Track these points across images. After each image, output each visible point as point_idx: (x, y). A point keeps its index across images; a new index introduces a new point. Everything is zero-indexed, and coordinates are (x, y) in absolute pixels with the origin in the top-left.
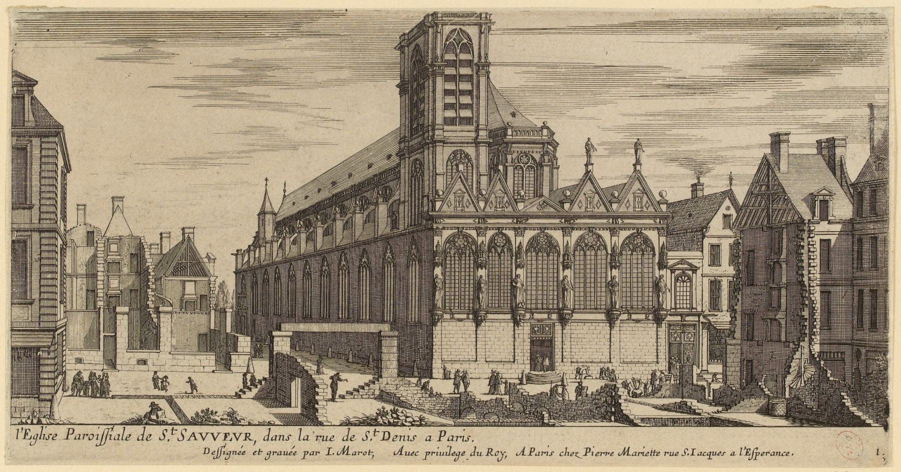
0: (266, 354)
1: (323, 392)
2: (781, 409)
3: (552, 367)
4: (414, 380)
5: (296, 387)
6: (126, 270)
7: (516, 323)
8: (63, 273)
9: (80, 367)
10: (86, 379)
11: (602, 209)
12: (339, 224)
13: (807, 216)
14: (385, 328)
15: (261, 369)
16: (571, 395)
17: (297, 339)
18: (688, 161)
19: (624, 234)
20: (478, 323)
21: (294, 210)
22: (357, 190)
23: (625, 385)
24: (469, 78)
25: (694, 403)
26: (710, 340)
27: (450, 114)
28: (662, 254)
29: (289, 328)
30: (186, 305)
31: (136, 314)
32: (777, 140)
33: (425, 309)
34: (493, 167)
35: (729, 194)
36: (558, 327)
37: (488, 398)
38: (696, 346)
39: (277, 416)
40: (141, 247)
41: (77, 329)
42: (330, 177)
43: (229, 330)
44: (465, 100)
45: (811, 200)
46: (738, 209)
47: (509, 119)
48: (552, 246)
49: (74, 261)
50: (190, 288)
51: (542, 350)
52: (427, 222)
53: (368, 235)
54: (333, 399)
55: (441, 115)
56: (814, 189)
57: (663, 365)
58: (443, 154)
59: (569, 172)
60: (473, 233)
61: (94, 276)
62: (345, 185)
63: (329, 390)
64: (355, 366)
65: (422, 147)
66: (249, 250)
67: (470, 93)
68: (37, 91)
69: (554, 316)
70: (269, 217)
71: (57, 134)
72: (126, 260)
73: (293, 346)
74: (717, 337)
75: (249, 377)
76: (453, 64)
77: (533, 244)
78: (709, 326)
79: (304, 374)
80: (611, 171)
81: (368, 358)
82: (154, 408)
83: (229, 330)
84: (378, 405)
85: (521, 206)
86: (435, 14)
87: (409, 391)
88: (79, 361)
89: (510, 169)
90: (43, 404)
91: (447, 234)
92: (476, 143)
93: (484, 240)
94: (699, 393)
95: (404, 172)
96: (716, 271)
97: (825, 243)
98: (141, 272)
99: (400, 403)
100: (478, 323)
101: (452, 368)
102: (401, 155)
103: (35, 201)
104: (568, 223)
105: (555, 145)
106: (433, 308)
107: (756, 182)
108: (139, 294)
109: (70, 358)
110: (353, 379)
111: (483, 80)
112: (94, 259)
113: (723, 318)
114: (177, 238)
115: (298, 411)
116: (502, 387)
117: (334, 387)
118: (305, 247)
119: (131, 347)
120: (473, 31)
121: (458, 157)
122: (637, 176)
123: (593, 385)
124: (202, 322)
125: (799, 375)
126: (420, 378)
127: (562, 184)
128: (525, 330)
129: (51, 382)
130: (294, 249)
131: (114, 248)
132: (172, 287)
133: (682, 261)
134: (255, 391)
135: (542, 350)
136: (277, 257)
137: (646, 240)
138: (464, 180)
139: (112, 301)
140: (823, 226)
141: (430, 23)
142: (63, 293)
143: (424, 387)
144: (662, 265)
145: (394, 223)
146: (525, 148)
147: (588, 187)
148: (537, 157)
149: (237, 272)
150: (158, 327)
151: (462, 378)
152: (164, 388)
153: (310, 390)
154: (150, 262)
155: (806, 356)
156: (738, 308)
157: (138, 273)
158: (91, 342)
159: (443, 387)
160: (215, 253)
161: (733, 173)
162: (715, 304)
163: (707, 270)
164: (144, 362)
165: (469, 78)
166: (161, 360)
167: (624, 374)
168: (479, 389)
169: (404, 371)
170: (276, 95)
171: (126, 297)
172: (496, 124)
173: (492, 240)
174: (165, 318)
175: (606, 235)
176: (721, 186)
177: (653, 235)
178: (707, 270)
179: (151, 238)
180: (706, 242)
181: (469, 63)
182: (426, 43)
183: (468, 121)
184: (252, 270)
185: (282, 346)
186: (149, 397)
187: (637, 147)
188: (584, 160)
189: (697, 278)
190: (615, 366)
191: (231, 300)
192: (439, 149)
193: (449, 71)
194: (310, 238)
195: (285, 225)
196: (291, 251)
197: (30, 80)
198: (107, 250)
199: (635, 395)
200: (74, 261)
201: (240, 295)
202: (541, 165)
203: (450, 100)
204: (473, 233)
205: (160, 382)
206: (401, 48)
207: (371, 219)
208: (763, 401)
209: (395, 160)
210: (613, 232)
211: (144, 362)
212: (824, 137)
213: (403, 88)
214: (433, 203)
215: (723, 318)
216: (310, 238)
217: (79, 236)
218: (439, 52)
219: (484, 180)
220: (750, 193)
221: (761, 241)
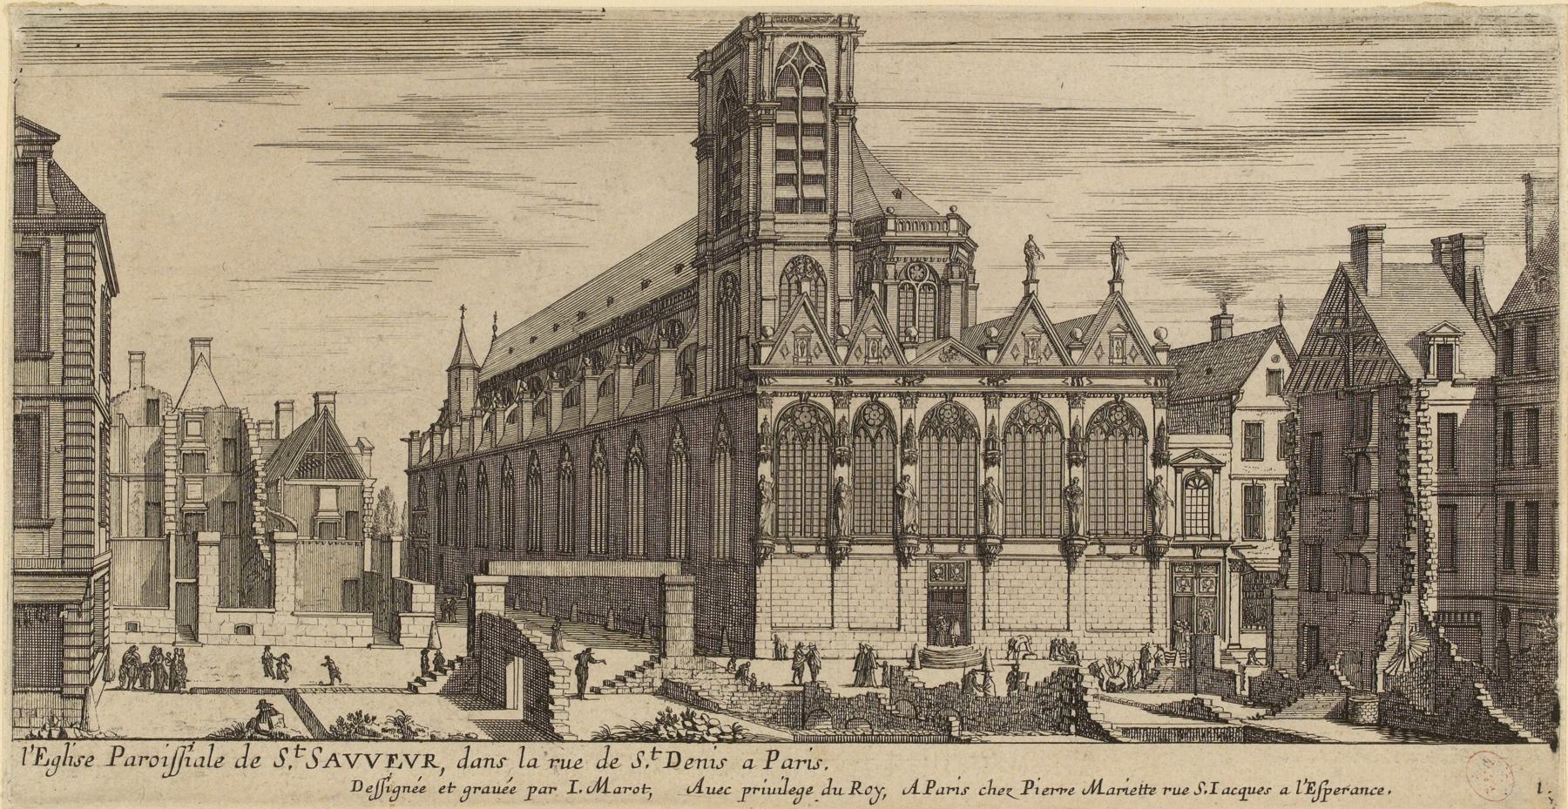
0: (462, 616)
1: (563, 683)
2: (1369, 713)
3: (965, 639)
4: (723, 661)
5: (515, 674)
6: (215, 467)
7: (903, 560)
8: (105, 473)
9: (134, 638)
10: (145, 659)
11: (1054, 360)
12: (591, 387)
13: (1415, 373)
14: (672, 569)
15: (454, 641)
16: (1000, 688)
17: (516, 590)
18: (1205, 276)
19: (1092, 405)
20: (835, 560)
22: (623, 326)
23: (1095, 670)
24: (820, 130)
25: (1216, 702)
27: (787, 192)
28: (1159, 439)
29: (502, 570)
30: (320, 529)
31: (233, 545)
32: (1362, 239)
33: (742, 536)
34: (862, 287)
35: (1277, 334)
36: (977, 568)
39: (481, 724)
40: (241, 427)
41: (129, 572)
42: (575, 304)
43: (396, 573)
44: (813, 168)
45: (1422, 344)
48: (965, 425)
49: (124, 451)
50: (328, 499)
51: (949, 609)
52: (744, 383)
53: (641, 405)
54: (580, 695)
56: (1426, 325)
57: (1162, 636)
58: (774, 263)
59: (995, 296)
60: (827, 403)
61: (160, 478)
62: (600, 318)
63: (574, 679)
65: (737, 250)
67: (821, 155)
68: (59, 153)
69: (970, 549)
70: (466, 375)
71: (94, 229)
72: (216, 450)
73: (509, 602)
74: (1257, 585)
75: (431, 655)
76: (791, 104)
77: (933, 422)
78: (1243, 566)
79: (529, 650)
80: (1070, 294)
81: (641, 622)
82: (265, 710)
83: (396, 573)
84: (659, 705)
86: (759, 17)
87: (714, 680)
88: (133, 627)
89: (892, 291)
91: (780, 403)
92: (833, 244)
94: (1225, 683)
95: (706, 295)
97: (1447, 419)
98: (242, 471)
100: (835, 560)
101: (790, 640)
102: (699, 264)
103: (56, 346)
104: (995, 384)
105: (972, 248)
107: (1325, 313)
110: (616, 660)
111: (844, 133)
112: (160, 443)
113: (1267, 553)
114: (304, 412)
115: (519, 715)
118: (530, 427)
119: (223, 603)
120: (826, 47)
121: (801, 268)
122: (1116, 302)
123: (1038, 670)
124: (350, 559)
125: (1401, 653)
126: (733, 658)
127: (983, 317)
128: (918, 573)
129: (83, 665)
130: (512, 430)
131: (194, 428)
132: (296, 498)
133: (1195, 452)
134: (442, 680)
135: (949, 609)
136: (481, 444)
137: (1132, 415)
138: (811, 309)
139: (192, 522)
140: (1444, 390)
141: (750, 33)
142: (104, 509)
143: (740, 674)
144: (1159, 459)
145: (688, 386)
146: (919, 252)
147: (1030, 320)
148: (940, 268)
149: (410, 472)
150: (271, 569)
151: (807, 658)
152: (282, 676)
154: (258, 454)
155: (1413, 618)
156: (1294, 534)
158: (154, 594)
159: (774, 674)
160: (371, 437)
163: (1239, 467)
164: (248, 630)
165: (820, 130)
166: (276, 625)
167: (1092, 650)
168: (837, 677)
169: (705, 645)
170: (481, 159)
171: (216, 516)
172: (866, 212)
173: (861, 414)
175: (1061, 405)
177: (1143, 406)
178: (1239, 467)
179: (260, 411)
180: (1238, 418)
181: (820, 103)
182: (744, 68)
183: (819, 205)
184: (438, 467)
185: (490, 601)
186: (255, 691)
187: (1116, 250)
189: (1221, 482)
190: (1077, 636)
191: (401, 521)
192: (767, 255)
193: (785, 117)
194: (540, 412)
195: (495, 389)
196: (507, 434)
197: (47, 133)
198: (182, 432)
199: (1112, 688)
200: (124, 451)
201: (416, 512)
203: (787, 168)
204: (827, 403)
205: (275, 665)
206: (699, 76)
207: (646, 378)
208: (1337, 699)
210: (1074, 400)
211: (248, 630)
212: (1445, 233)
213: (703, 147)
214: (757, 349)
215: (1267, 553)
216: (540, 412)
217: (132, 407)
218: (766, 84)
219: (846, 309)
220: (1315, 332)
221: (1334, 416)
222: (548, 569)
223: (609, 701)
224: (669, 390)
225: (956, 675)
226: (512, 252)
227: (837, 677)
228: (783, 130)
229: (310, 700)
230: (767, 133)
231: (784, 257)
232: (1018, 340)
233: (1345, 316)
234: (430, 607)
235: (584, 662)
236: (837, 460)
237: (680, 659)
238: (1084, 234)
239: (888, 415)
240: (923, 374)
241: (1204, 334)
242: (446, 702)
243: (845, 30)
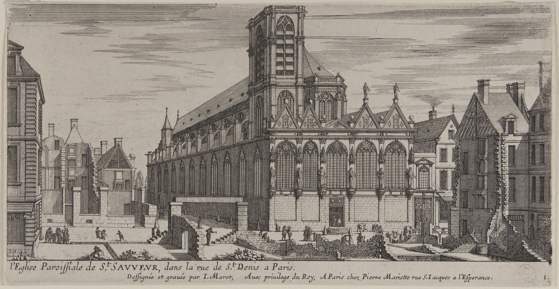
0: (166, 217)
1: (202, 240)
2: (484, 251)
3: (343, 224)
5: (185, 237)
6: (79, 164)
7: (321, 197)
9: (50, 224)
10: (54, 232)
11: (374, 127)
12: (212, 136)
13: (500, 131)
14: (240, 200)
15: (163, 225)
16: (355, 241)
17: (185, 207)
18: (427, 97)
19: (387, 142)
20: (297, 197)
21: (184, 127)
22: (223, 115)
23: (388, 235)
24: (292, 46)
25: (430, 247)
27: (280, 68)
28: (411, 155)
29: (180, 200)
30: (116, 186)
31: (86, 192)
32: (482, 84)
33: (265, 188)
34: (306, 102)
35: (452, 118)
36: (346, 200)
39: (173, 254)
40: (88, 150)
41: (49, 201)
42: (206, 107)
43: (143, 201)
44: (289, 59)
45: (503, 121)
48: (343, 149)
49: (47, 159)
50: (119, 175)
51: (337, 214)
52: (266, 135)
53: (229, 143)
56: (505, 114)
57: (411, 223)
58: (276, 93)
59: (353, 104)
60: (294, 142)
62: (215, 112)
63: (206, 238)
64: (221, 223)
65: (263, 88)
67: (292, 55)
68: (24, 53)
69: (344, 193)
70: (168, 132)
71: (36, 80)
72: (80, 158)
73: (183, 212)
74: (445, 206)
75: (156, 230)
77: (331, 149)
78: (440, 199)
79: (190, 228)
80: (379, 104)
81: (231, 220)
82: (97, 250)
83: (143, 201)
84: (236, 247)
85: (323, 125)
86: (270, 7)
87: (255, 239)
88: (50, 221)
89: (317, 102)
90: (27, 248)
91: (278, 142)
92: (296, 86)
93: (301, 146)
94: (434, 240)
95: (252, 104)
97: (512, 148)
98: (89, 165)
100: (297, 197)
101: (281, 225)
102: (249, 93)
103: (22, 122)
104: (353, 135)
105: (345, 87)
107: (469, 110)
108: (87, 180)
110: (220, 232)
111: (300, 47)
112: (60, 156)
113: (448, 194)
114: (111, 145)
118: (190, 150)
119: (82, 212)
120: (294, 17)
121: (285, 95)
122: (395, 106)
123: (368, 236)
124: (126, 196)
125: (496, 230)
126: (261, 231)
127: (349, 112)
128: (326, 202)
129: (32, 234)
130: (184, 151)
132: (108, 175)
133: (423, 159)
134: (159, 239)
135: (337, 214)
136: (173, 156)
137: (401, 146)
139: (71, 184)
140: (511, 137)
141: (267, 12)
142: (40, 179)
143: (264, 237)
144: (410, 162)
145: (246, 135)
146: (326, 89)
147: (365, 113)
148: (334, 95)
150: (99, 200)
151: (287, 231)
152: (103, 238)
153: (194, 238)
155: (500, 217)
156: (458, 188)
157: (87, 166)
158: (57, 209)
159: (276, 236)
160: (134, 153)
161: (455, 104)
163: (439, 164)
164: (91, 222)
165: (292, 46)
166: (100, 220)
167: (387, 229)
168: (298, 238)
169: (251, 227)
170: (173, 56)
171: (79, 181)
172: (308, 75)
173: (306, 146)
174: (103, 194)
175: (376, 143)
176: (448, 113)
177: (405, 143)
178: (439, 164)
179: (95, 144)
180: (438, 147)
181: (292, 37)
182: (265, 24)
183: (291, 72)
184: (158, 164)
186: (93, 243)
187: (395, 88)
189: (432, 169)
190: (382, 223)
191: (145, 183)
193: (280, 42)
194: (194, 145)
195: (178, 137)
196: (182, 153)
197: (19, 46)
198: (68, 152)
199: (394, 242)
200: (47, 159)
201: (150, 180)
203: (280, 59)
205: (101, 234)
206: (250, 27)
207: (231, 133)
208: (473, 246)
210: (381, 141)
211: (91, 222)
212: (511, 82)
213: (251, 52)
214: (270, 123)
215: (448, 194)
216: (194, 145)
217: (50, 143)
218: (273, 30)
219: (301, 109)
220: (465, 117)
221: (472, 146)
222: (197, 200)
224: (239, 137)
228: (279, 46)
230: (273, 47)
235: (209, 233)
236: (298, 162)
237: (243, 231)
239: (316, 146)
242: (161, 247)
243: (301, 11)
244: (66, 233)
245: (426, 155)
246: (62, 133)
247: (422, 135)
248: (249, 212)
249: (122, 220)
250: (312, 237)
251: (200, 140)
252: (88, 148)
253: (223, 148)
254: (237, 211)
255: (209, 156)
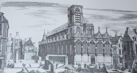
0: (44, 60)
1: (55, 67)
2: (132, 71)
3: (95, 63)
4: (71, 65)
5: (50, 66)
6: (18, 45)
7: (89, 56)
8: (7, 46)
9: (9, 63)
10: (10, 65)
11: (102, 38)
12: (58, 38)
13: (133, 40)
14: (66, 56)
15: (43, 63)
16: (98, 68)
17: (50, 57)
18: (114, 31)
19: (105, 42)
20: (82, 55)
21: (50, 35)
22: (61, 32)
23: (107, 67)
24: (79, 16)
25: (118, 70)
26: (120, 59)
27: (77, 21)
28: (111, 45)
29: (48, 55)
30: (29, 51)
31: (20, 53)
32: (127, 28)
33: (73, 53)
34: (84, 30)
35: (121, 36)
36: (95, 57)
37: (84, 68)
38: (117, 60)
39: (46, 71)
40: (21, 41)
41: (9, 55)
42: (56, 30)
43: (37, 56)
44: (79, 19)
45: (133, 38)
46: (122, 39)
47: (86, 22)
48: (94, 43)
49: (9, 43)
50: (30, 48)
51: (93, 60)
52: (73, 38)
53: (63, 39)
54: (56, 68)
55: (75, 21)
56: (134, 36)
57: (113, 63)
58: (75, 27)
59: (96, 32)
60: (81, 40)
61: (12, 46)
62: (58, 31)
63: (56, 67)
64: (61, 63)
65: (72, 26)
66: (41, 42)
67: (80, 18)
68: (4, 15)
69: (95, 55)
70: (45, 36)
71: (7, 22)
72: (19, 43)
73: (49, 59)
74: (121, 59)
75: (41, 64)
76: (76, 13)
77: (91, 43)
78: (119, 57)
79: (51, 64)
80: (103, 32)
81: (63, 61)
82: (23, 70)
83: (37, 56)
84: (65, 69)
85: (88, 36)
86: (74, 5)
87: (70, 67)
88: (9, 61)
89: (86, 30)
90: (2, 70)
91: (76, 40)
92: (81, 26)
93: (82, 41)
94: (119, 68)
95: (69, 30)
96: (120, 48)
97: (136, 45)
98: (21, 46)
99: (69, 69)
100: (82, 55)
101: (78, 63)
102: (68, 27)
103: (2, 33)
104: (96, 39)
105: (94, 27)
106: (74, 53)
107: (125, 35)
108: (21, 49)
109: (7, 61)
110: (60, 65)
111: (82, 16)
112: (12, 43)
113: (121, 56)
114: (28, 39)
115: (50, 70)
116: (86, 66)
117: (57, 66)
118: (51, 41)
119: (19, 59)
120: (80, 8)
121: (78, 28)
122: (107, 32)
123: (102, 66)
124: (32, 54)
125: (134, 66)
126: (72, 65)
127: (95, 33)
128: (90, 57)
129: (3, 66)
130: (50, 42)
131: (16, 41)
132: (27, 48)
133: (115, 46)
134: (42, 67)
135: (93, 60)
136: (46, 43)
137: (109, 43)
138: (79, 32)
139: (16, 50)
140: (135, 42)
141: (73, 6)
142: (7, 49)
143: (73, 66)
144: (111, 47)
145: (67, 38)
146: (89, 27)
147: (99, 34)
148: (91, 29)
149: (39, 46)
150: (24, 55)
151: (79, 65)
152: (25, 66)
153: (52, 66)
154: (23, 43)
155: (135, 62)
156: (124, 54)
157: (21, 46)
158: (11, 58)
159: (76, 66)
160: (35, 42)
161: (122, 33)
162: (120, 54)
163: (118, 48)
164: (21, 62)
165: (79, 16)
166: (24, 61)
167: (107, 65)
168: (83, 67)
169: (69, 63)
170: (46, 16)
171: (18, 50)
172: (84, 23)
173: (84, 41)
174: (25, 54)
175: (102, 41)
176: (120, 35)
177: (110, 42)
178: (118, 48)
179: (23, 39)
180: (118, 43)
181: (80, 13)
182: (72, 10)
183: (80, 22)
184: (42, 45)
185: (47, 59)
186: (22, 68)
187: (107, 28)
188: (98, 30)
189: (117, 49)
190: (105, 63)
191: (38, 50)
192: (75, 26)
193: (76, 14)
194: (56, 39)
195: (48, 38)
196: (49, 42)
197: (2, 13)
198: (15, 42)
199: (108, 68)
200: (9, 43)
201: (40, 50)
202: (91, 30)
203: (76, 19)
204: (81, 40)
205: (24, 65)
206: (68, 10)
207: (63, 37)
208: (129, 70)
209: (67, 28)
210: (104, 41)
211: (21, 62)
212: (134, 28)
213: (68, 16)
214: (74, 35)
215: (121, 56)
216: (56, 39)
217: (10, 39)
218: (74, 11)
219: (82, 32)
220: (124, 36)
221: (126, 44)
222: (53, 55)
223: (59, 69)
224: (65, 38)
225: (94, 67)
226: (50, 25)
227: (83, 67)
228: (76, 15)
229: (28, 69)
230: (75, 15)
231: (76, 27)
232: (98, 35)
233: (126, 36)
234: (41, 59)
235: (57, 65)
236: (82, 46)
237: (67, 65)
238: (104, 26)
239: (87, 42)
240: (89, 38)
241: (115, 36)
242: (42, 69)
243: (81, 7)
244: (13, 65)
245: (115, 45)
246: (14, 36)
247: (114, 40)
248: (68, 60)
249: (30, 61)
250: (86, 66)
251: (54, 39)
252: (21, 40)
253: (61, 41)
254: (65, 59)
255: (51, 44)
